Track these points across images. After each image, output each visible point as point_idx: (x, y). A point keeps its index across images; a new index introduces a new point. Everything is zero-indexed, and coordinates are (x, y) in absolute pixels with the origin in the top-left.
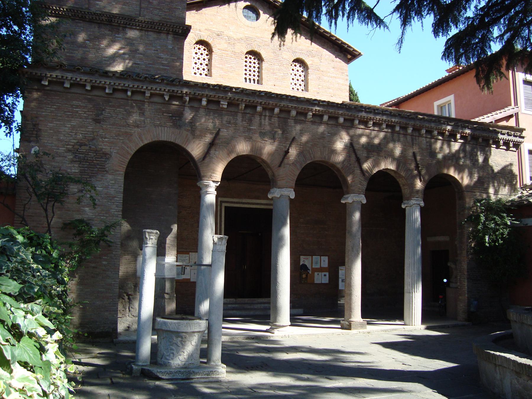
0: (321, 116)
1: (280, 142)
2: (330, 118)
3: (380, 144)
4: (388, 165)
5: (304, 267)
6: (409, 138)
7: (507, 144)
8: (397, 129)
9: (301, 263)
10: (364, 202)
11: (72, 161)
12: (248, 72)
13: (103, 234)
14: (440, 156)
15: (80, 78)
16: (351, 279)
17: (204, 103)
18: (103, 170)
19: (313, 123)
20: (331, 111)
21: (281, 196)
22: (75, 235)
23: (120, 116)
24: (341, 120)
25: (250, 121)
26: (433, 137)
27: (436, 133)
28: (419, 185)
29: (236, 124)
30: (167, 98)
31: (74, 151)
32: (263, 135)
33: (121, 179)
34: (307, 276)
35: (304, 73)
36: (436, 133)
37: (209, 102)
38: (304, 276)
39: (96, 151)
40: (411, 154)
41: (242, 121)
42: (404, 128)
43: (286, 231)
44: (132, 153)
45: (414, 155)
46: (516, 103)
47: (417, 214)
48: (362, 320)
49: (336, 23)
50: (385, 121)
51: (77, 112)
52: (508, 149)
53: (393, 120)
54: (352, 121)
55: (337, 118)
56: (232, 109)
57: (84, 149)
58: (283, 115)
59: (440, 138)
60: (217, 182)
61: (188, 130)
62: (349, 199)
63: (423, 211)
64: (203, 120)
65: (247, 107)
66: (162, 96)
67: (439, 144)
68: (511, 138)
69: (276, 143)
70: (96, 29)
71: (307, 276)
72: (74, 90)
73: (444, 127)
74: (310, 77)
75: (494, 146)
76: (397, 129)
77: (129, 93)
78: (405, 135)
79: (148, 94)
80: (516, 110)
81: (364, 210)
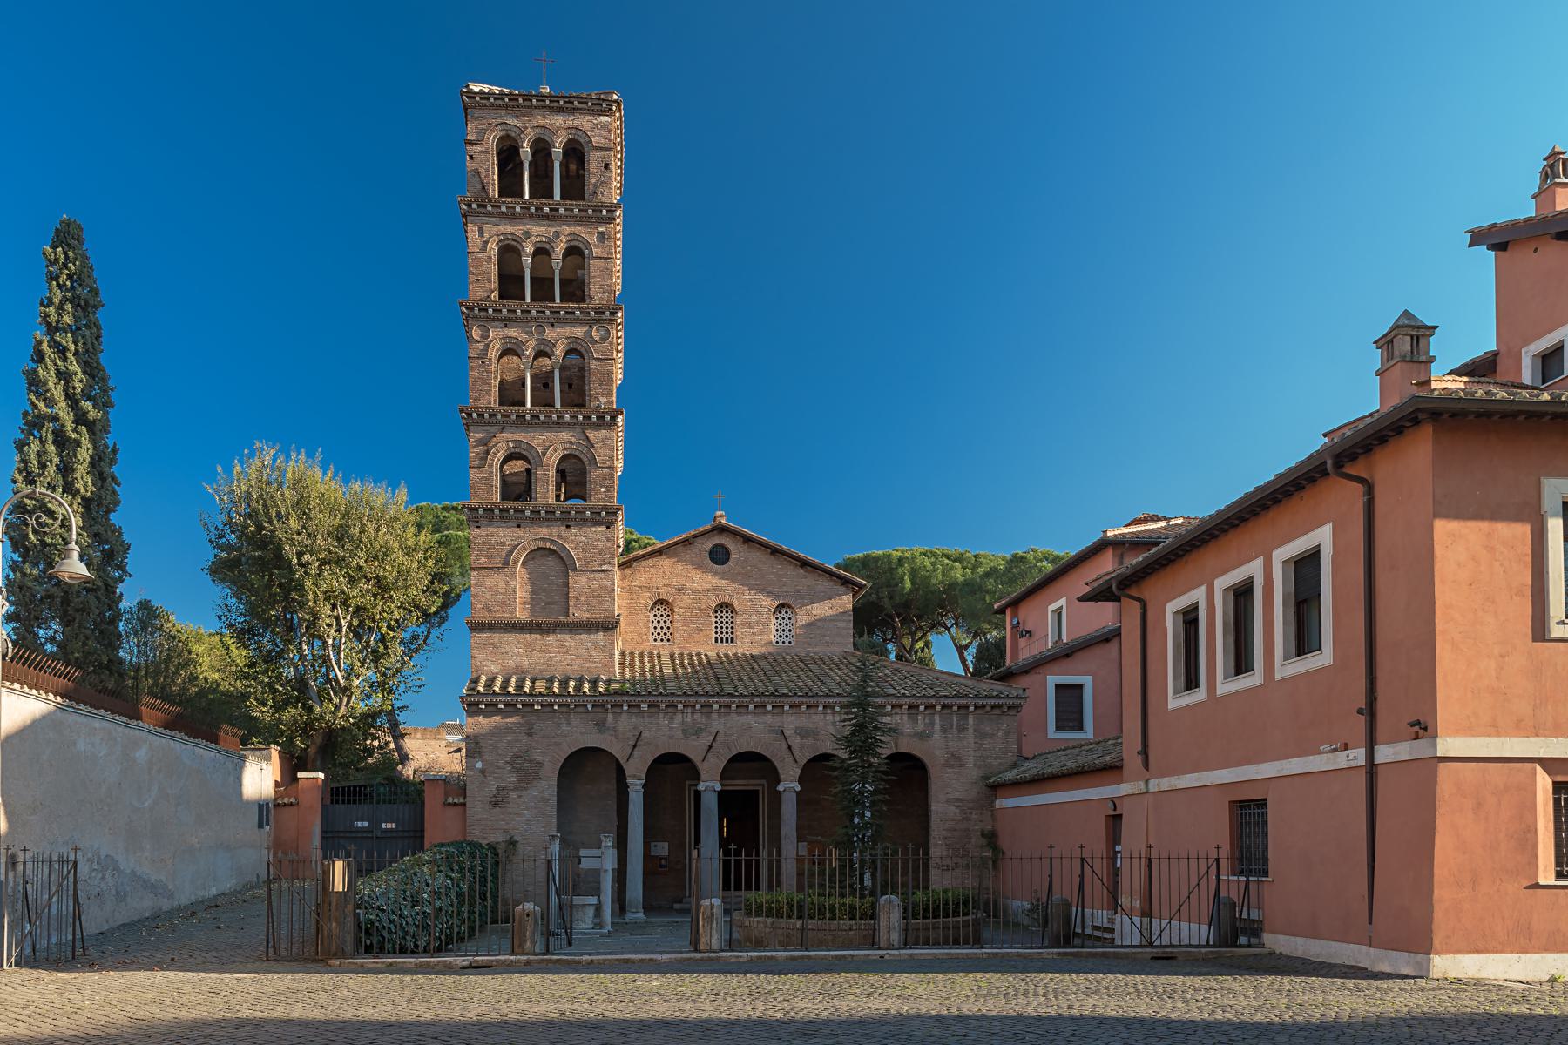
8: (837, 709)
10: (798, 789)
11: (511, 772)
12: (719, 630)
57: (519, 761)
76: (837, 709)
77: (556, 707)
79: (572, 707)
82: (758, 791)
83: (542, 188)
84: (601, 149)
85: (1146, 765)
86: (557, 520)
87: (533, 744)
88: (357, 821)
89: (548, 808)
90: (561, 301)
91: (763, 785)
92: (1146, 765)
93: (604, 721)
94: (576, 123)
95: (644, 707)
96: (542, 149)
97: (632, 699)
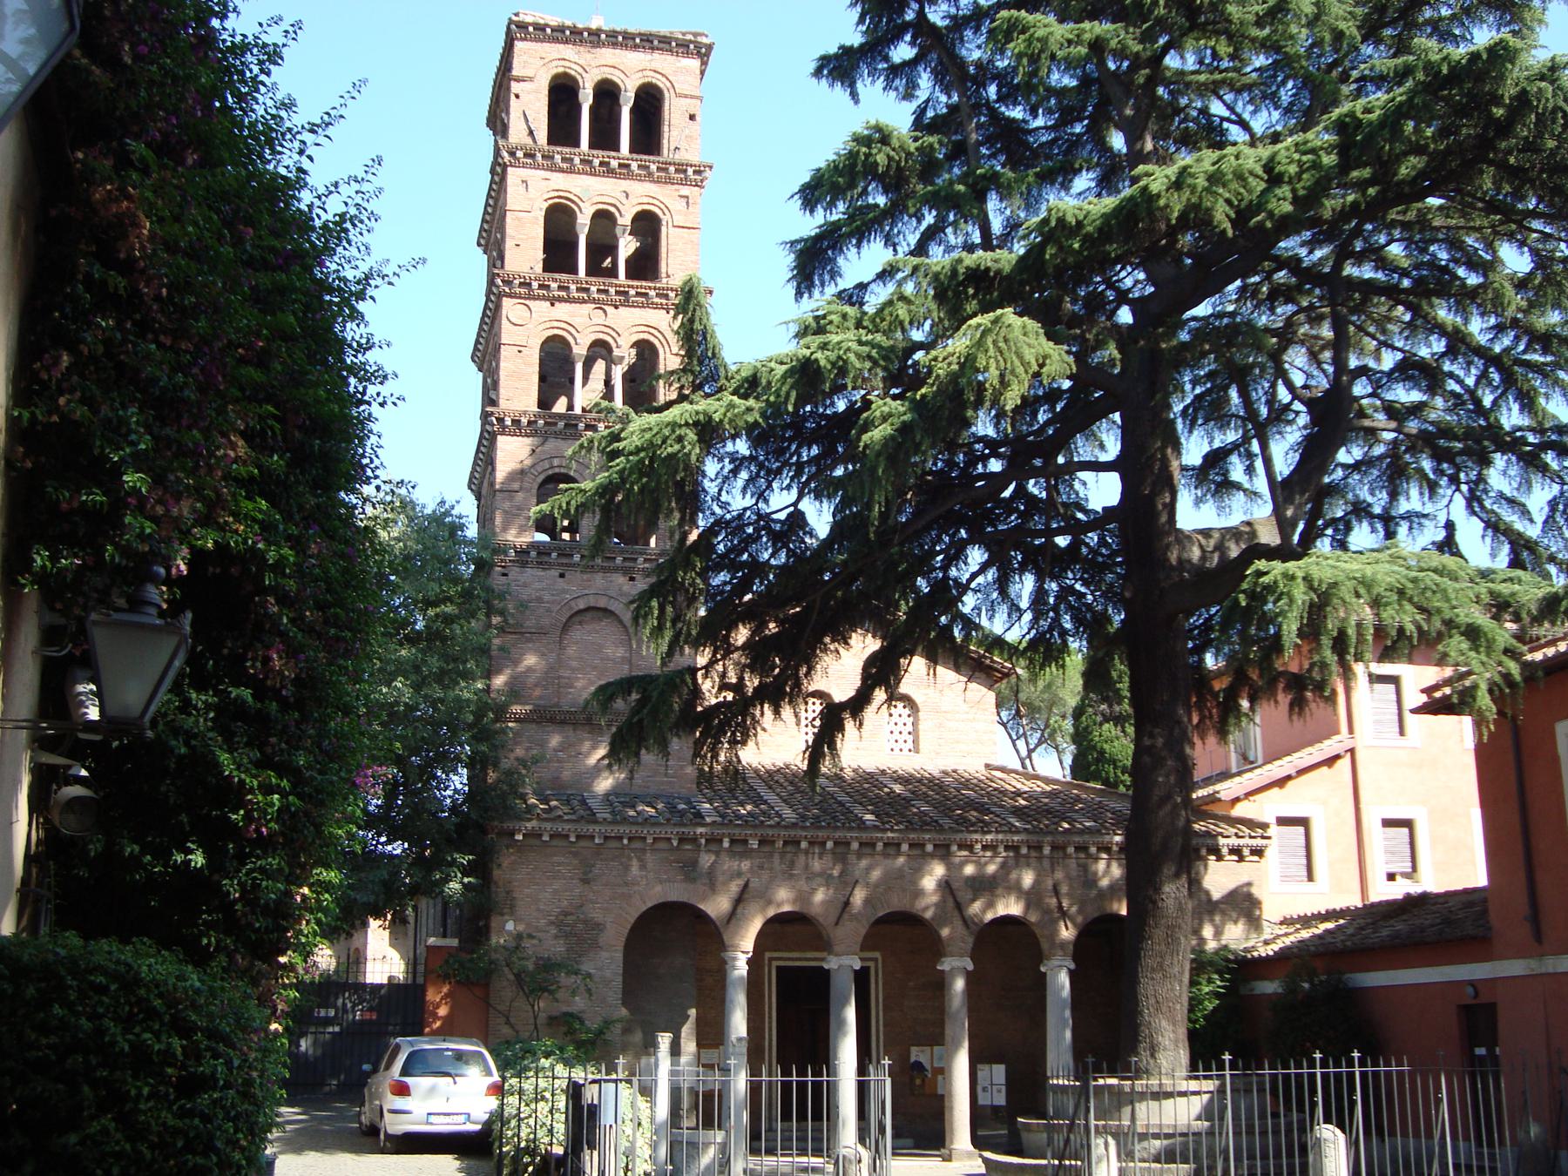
0: (898, 845)
1: (836, 889)
4: (1011, 907)
5: (919, 1066)
7: (1236, 851)
8: (1024, 851)
9: (913, 1059)
11: (556, 937)
16: (951, 1084)
17: (726, 844)
18: (595, 946)
20: (911, 836)
22: (566, 1034)
23: (614, 873)
24: (929, 848)
25: (792, 864)
27: (1093, 850)
29: (771, 869)
30: (675, 843)
31: (558, 924)
33: (619, 956)
34: (923, 1081)
35: (911, 719)
36: (1093, 850)
37: (732, 842)
38: (918, 1082)
39: (585, 922)
41: (781, 863)
46: (1351, 730)
47: (1064, 979)
48: (971, 1148)
49: (935, 674)
50: (1002, 841)
51: (559, 871)
53: (1016, 838)
54: (948, 847)
56: (766, 849)
58: (840, 849)
59: (1105, 856)
60: (747, 953)
61: (705, 885)
62: (946, 965)
63: (1072, 974)
65: (786, 843)
70: (571, 733)
71: (923, 1081)
72: (555, 842)
73: (1107, 838)
74: (921, 727)
75: (1213, 858)
76: (1024, 851)
77: (625, 841)
78: (1040, 858)
79: (650, 841)
80: (1348, 744)
81: (971, 978)
83: (605, 137)
85: (1538, 935)
86: (616, 569)
87: (591, 896)
88: (319, 1007)
89: (610, 994)
91: (876, 960)
92: (1538, 935)
93: (694, 864)
94: (654, 65)
95: (754, 844)
97: (737, 831)
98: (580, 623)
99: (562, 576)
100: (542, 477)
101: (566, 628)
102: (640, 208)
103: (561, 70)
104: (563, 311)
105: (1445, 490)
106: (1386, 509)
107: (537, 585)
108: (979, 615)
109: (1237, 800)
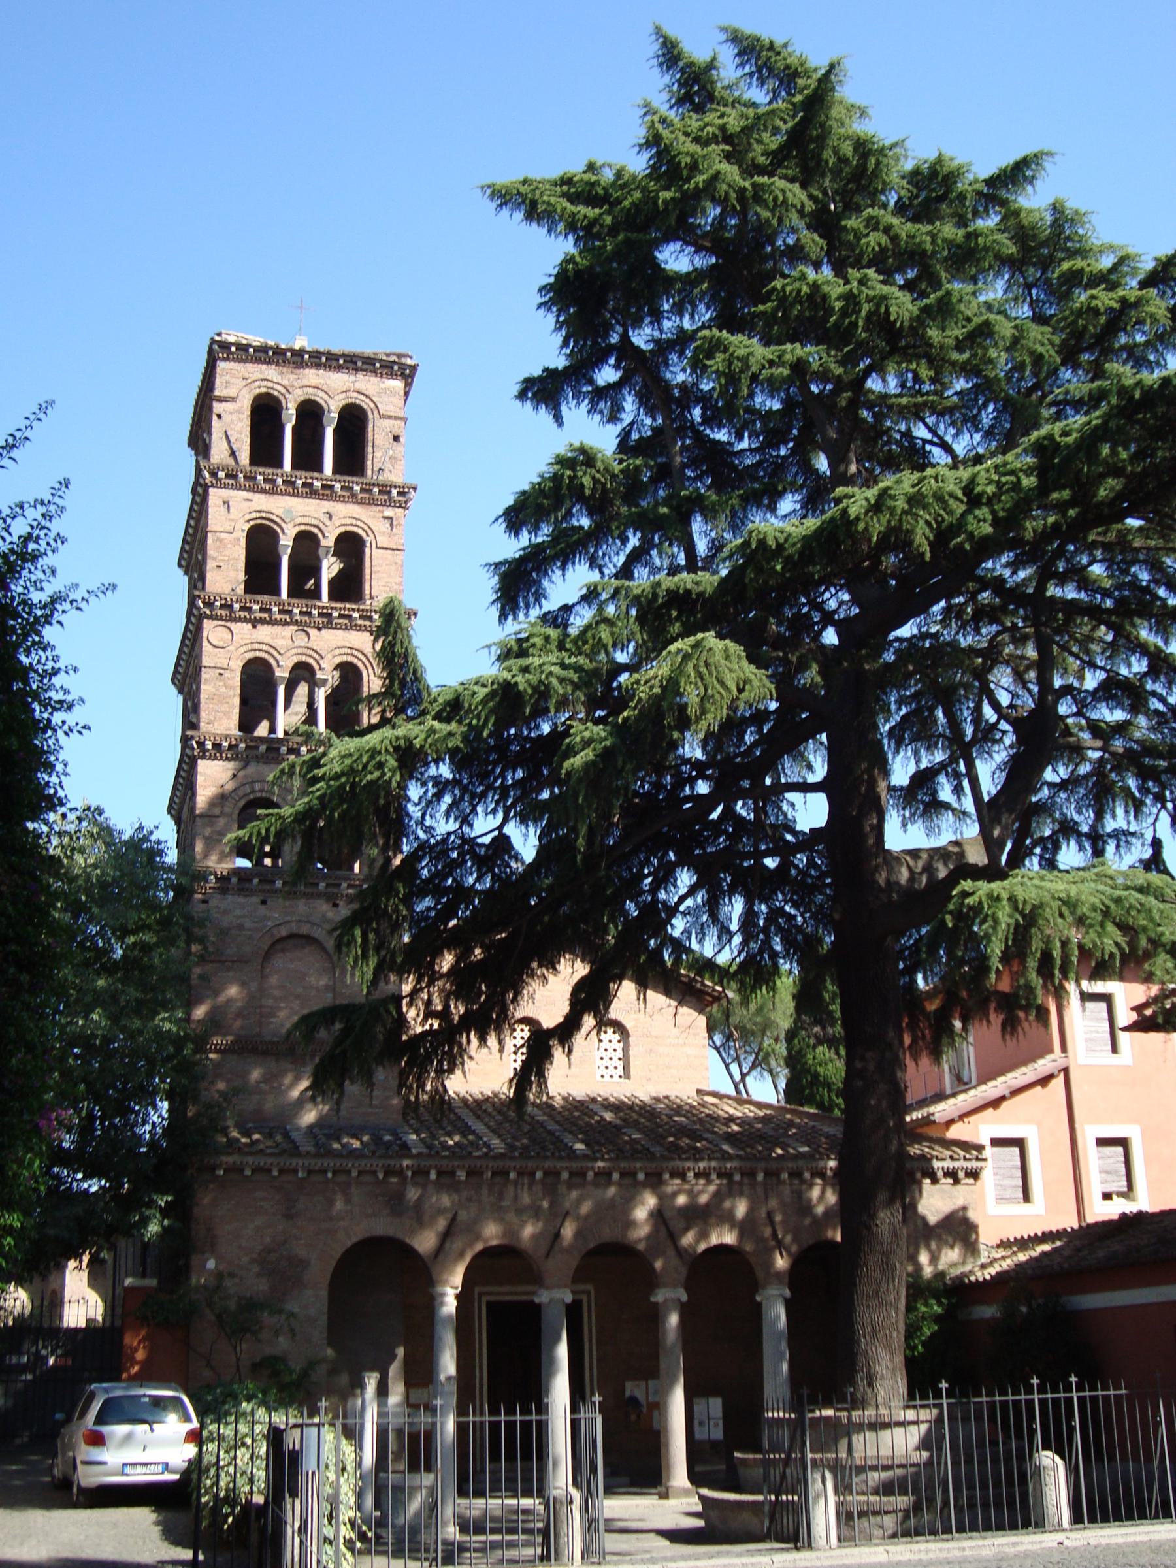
0: (609, 1174)
2: (623, 1175)
3: (707, 1205)
4: (727, 1237)
5: (633, 1401)
6: (760, 1190)
7: (952, 1174)
8: (737, 1178)
9: (628, 1393)
11: (259, 1275)
13: (305, 1374)
14: (820, 1210)
15: (262, 1161)
17: (433, 1175)
19: (595, 1185)
21: (551, 1301)
24: (641, 1176)
25: (501, 1196)
26: (803, 1181)
27: (807, 1175)
28: (781, 1262)
30: (381, 1176)
32: (519, 1211)
33: (324, 1293)
37: (439, 1174)
38: (633, 1417)
40: (764, 1215)
42: (752, 1174)
43: (562, 1351)
44: (337, 1256)
45: (770, 1216)
52: (957, 1181)
55: (634, 1175)
64: (434, 1200)
66: (374, 1173)
67: (816, 1193)
68: (957, 1164)
69: (540, 1224)
73: (821, 1164)
76: (737, 1178)
77: (330, 1175)
78: (754, 1184)
79: (354, 1174)
81: (686, 1311)
82: (489, 1304)
83: (308, 458)
84: (390, 417)
86: (319, 895)
90: (331, 598)
91: (480, 1295)
94: (358, 386)
95: (462, 1175)
96: (310, 413)
97: (444, 1162)
98: (283, 950)
99: (264, 902)
100: (242, 803)
101: (267, 956)
102: (343, 529)
103: (263, 390)
104: (265, 633)
105: (1151, 808)
106: (1093, 827)
107: (238, 912)
108: (689, 938)
109: (951, 1122)
